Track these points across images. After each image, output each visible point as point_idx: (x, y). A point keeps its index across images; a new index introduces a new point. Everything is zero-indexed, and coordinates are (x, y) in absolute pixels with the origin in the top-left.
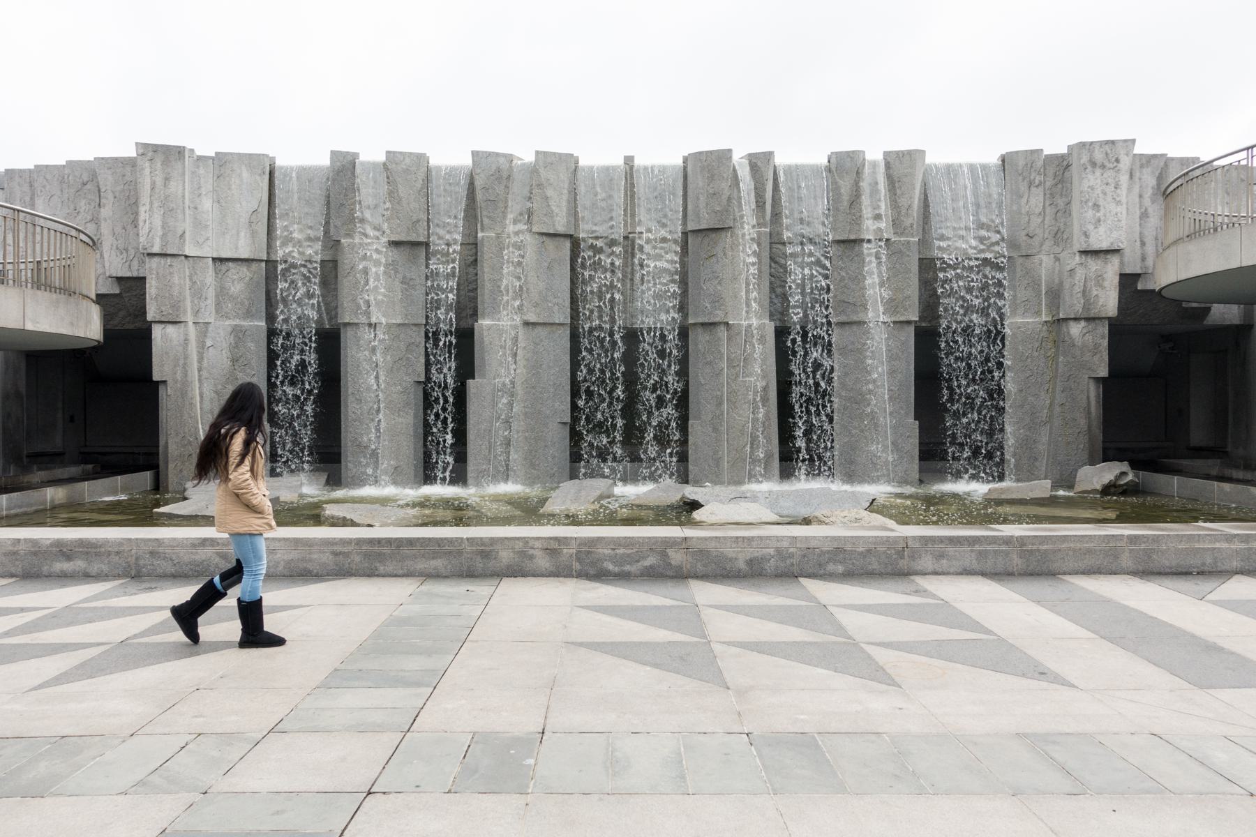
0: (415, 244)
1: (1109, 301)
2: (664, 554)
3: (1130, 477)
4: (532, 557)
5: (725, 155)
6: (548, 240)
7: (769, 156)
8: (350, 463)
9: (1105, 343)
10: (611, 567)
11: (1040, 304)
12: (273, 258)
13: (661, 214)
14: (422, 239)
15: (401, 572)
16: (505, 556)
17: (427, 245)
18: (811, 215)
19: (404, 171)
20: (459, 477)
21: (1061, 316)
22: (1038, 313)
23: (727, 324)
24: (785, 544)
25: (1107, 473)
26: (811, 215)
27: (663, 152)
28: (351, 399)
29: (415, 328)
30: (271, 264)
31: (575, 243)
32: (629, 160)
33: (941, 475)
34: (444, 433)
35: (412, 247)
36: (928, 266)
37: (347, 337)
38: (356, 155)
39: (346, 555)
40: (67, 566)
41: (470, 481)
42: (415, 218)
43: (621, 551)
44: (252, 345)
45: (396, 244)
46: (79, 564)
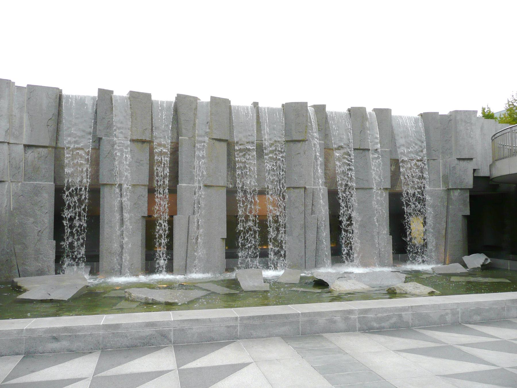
0: (143, 142)
1: (469, 182)
2: (400, 316)
3: (489, 261)
4: (335, 322)
5: (304, 105)
6: (217, 143)
7: (323, 107)
8: (104, 263)
9: (468, 200)
10: (375, 325)
11: (440, 182)
12: (59, 145)
13: (420, 149)
14: (148, 139)
15: (265, 335)
16: (322, 321)
17: (150, 142)
18: (342, 135)
19: (140, 101)
20: (170, 269)
21: (450, 187)
22: (440, 187)
23: (305, 188)
24: (455, 307)
25: (477, 260)
26: (342, 135)
27: (273, 100)
28: (106, 226)
29: (143, 187)
30: (56, 148)
31: (230, 145)
32: (256, 104)
33: (405, 261)
34: (156, 246)
35: (144, 142)
36: (396, 163)
37: (105, 192)
38: (112, 92)
39: (235, 327)
40: (55, 345)
41: (174, 272)
42: (145, 128)
43: (379, 315)
44: (46, 195)
45: (132, 141)
46: (65, 344)
